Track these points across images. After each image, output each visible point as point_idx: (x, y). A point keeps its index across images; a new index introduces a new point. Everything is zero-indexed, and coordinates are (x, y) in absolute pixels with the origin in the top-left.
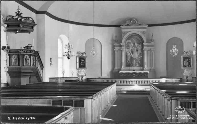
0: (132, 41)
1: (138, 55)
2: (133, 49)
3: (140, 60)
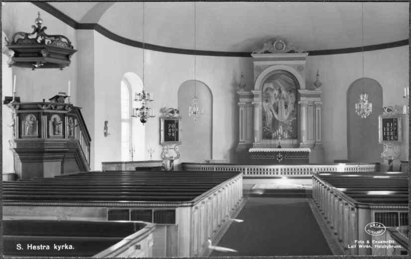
0: (275, 85)
1: (288, 114)
2: (278, 103)
3: (292, 126)
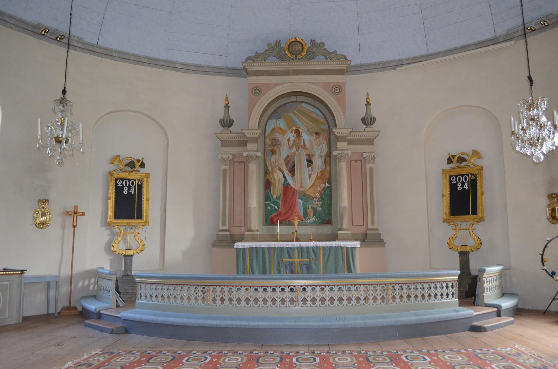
0: (290, 123)
1: (314, 177)
2: (293, 155)
3: (322, 199)
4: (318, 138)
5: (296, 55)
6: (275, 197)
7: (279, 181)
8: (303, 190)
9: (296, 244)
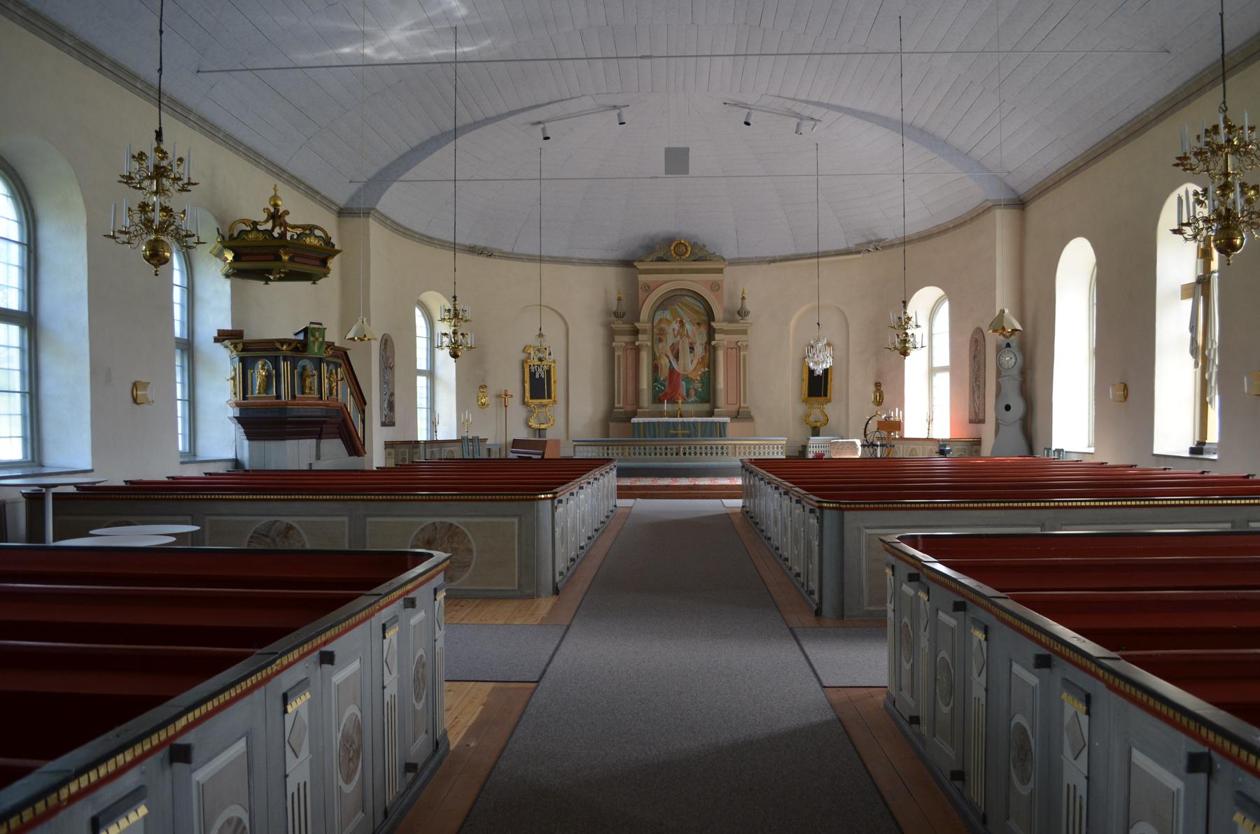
0: (675, 315)
1: (695, 362)
3: (702, 381)
4: (699, 328)
5: (681, 255)
6: (662, 379)
7: (666, 366)
8: (686, 373)
9: (680, 420)
